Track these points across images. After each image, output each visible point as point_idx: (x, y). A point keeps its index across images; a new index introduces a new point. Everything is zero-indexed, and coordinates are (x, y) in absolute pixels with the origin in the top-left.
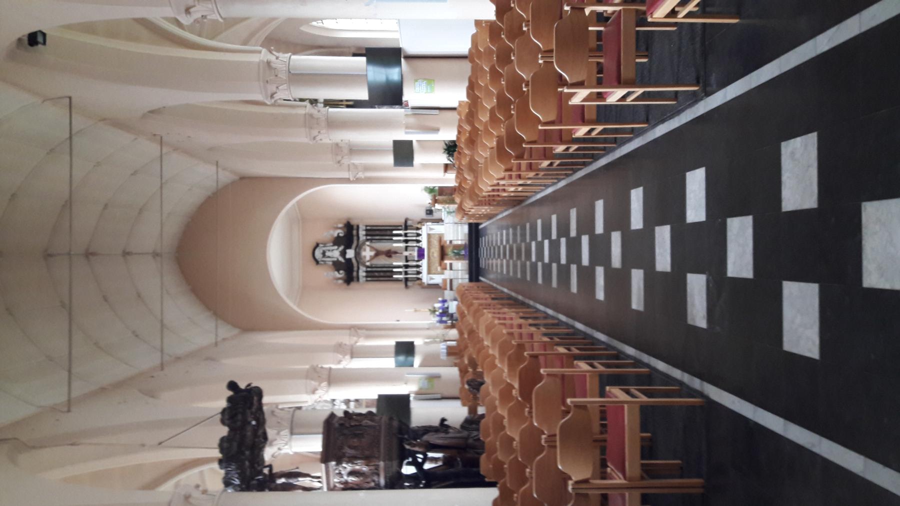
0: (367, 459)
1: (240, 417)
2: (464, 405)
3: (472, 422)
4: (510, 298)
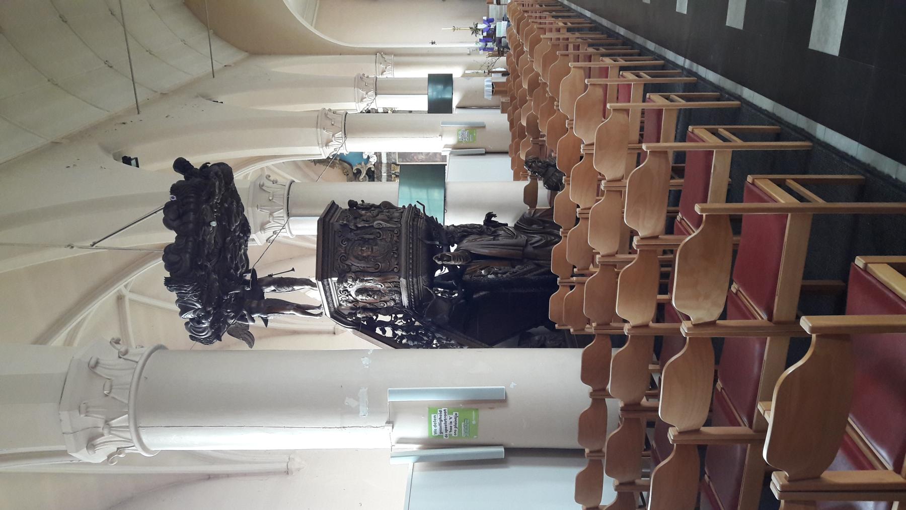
0: (381, 274)
1: (192, 216)
2: (503, 112)
3: (539, 224)
4: (595, 27)
